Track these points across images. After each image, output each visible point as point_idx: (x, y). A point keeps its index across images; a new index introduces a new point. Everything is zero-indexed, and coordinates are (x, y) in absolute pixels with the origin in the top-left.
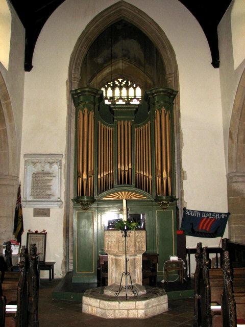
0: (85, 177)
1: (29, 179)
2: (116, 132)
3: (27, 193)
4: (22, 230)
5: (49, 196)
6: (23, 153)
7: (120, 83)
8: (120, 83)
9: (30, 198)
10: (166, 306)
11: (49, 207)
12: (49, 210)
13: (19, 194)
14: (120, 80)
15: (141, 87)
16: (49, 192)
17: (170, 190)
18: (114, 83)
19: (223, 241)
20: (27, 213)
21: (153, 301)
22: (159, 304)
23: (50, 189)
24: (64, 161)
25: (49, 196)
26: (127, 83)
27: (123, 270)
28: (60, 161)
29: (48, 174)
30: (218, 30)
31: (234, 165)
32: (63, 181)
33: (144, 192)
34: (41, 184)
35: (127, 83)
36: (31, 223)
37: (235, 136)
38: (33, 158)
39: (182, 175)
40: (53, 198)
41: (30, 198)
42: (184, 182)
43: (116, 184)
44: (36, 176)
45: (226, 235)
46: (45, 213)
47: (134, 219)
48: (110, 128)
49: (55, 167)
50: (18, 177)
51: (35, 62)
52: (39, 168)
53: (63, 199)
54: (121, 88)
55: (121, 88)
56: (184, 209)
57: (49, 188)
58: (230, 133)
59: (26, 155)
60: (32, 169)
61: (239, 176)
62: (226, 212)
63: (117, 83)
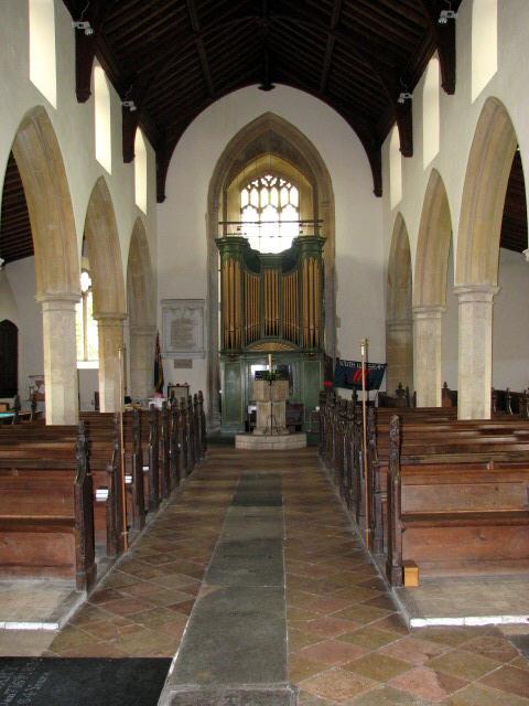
0: (232, 329)
1: (169, 328)
2: (262, 281)
3: (166, 343)
4: (163, 383)
5: (190, 346)
6: (159, 299)
7: (269, 183)
8: (269, 183)
9: (170, 349)
10: (305, 443)
11: (188, 358)
12: (190, 361)
13: (158, 345)
14: (269, 178)
15: (298, 188)
16: (189, 341)
17: (317, 340)
18: (260, 183)
19: (380, 394)
20: (168, 364)
21: (294, 438)
22: (299, 441)
23: (191, 338)
24: (206, 308)
25: (190, 346)
26: (278, 182)
27: (269, 413)
28: (202, 308)
29: (189, 322)
30: (382, 151)
31: (392, 312)
32: (206, 329)
33: (294, 345)
34: (181, 332)
35: (278, 182)
36: (173, 375)
37: (393, 281)
38: (172, 304)
39: (335, 322)
40: (193, 348)
41: (170, 349)
42: (338, 329)
43: (263, 335)
44: (175, 323)
45: (383, 388)
46: (187, 364)
47: (283, 373)
48: (256, 278)
49: (197, 313)
50: (155, 326)
51: (168, 191)
52: (179, 315)
53: (206, 349)
54: (269, 188)
55: (269, 188)
56: (338, 359)
57: (190, 337)
58: (389, 279)
59: (163, 301)
60: (171, 317)
61: (469, 292)
62: (384, 362)
63: (264, 182)
